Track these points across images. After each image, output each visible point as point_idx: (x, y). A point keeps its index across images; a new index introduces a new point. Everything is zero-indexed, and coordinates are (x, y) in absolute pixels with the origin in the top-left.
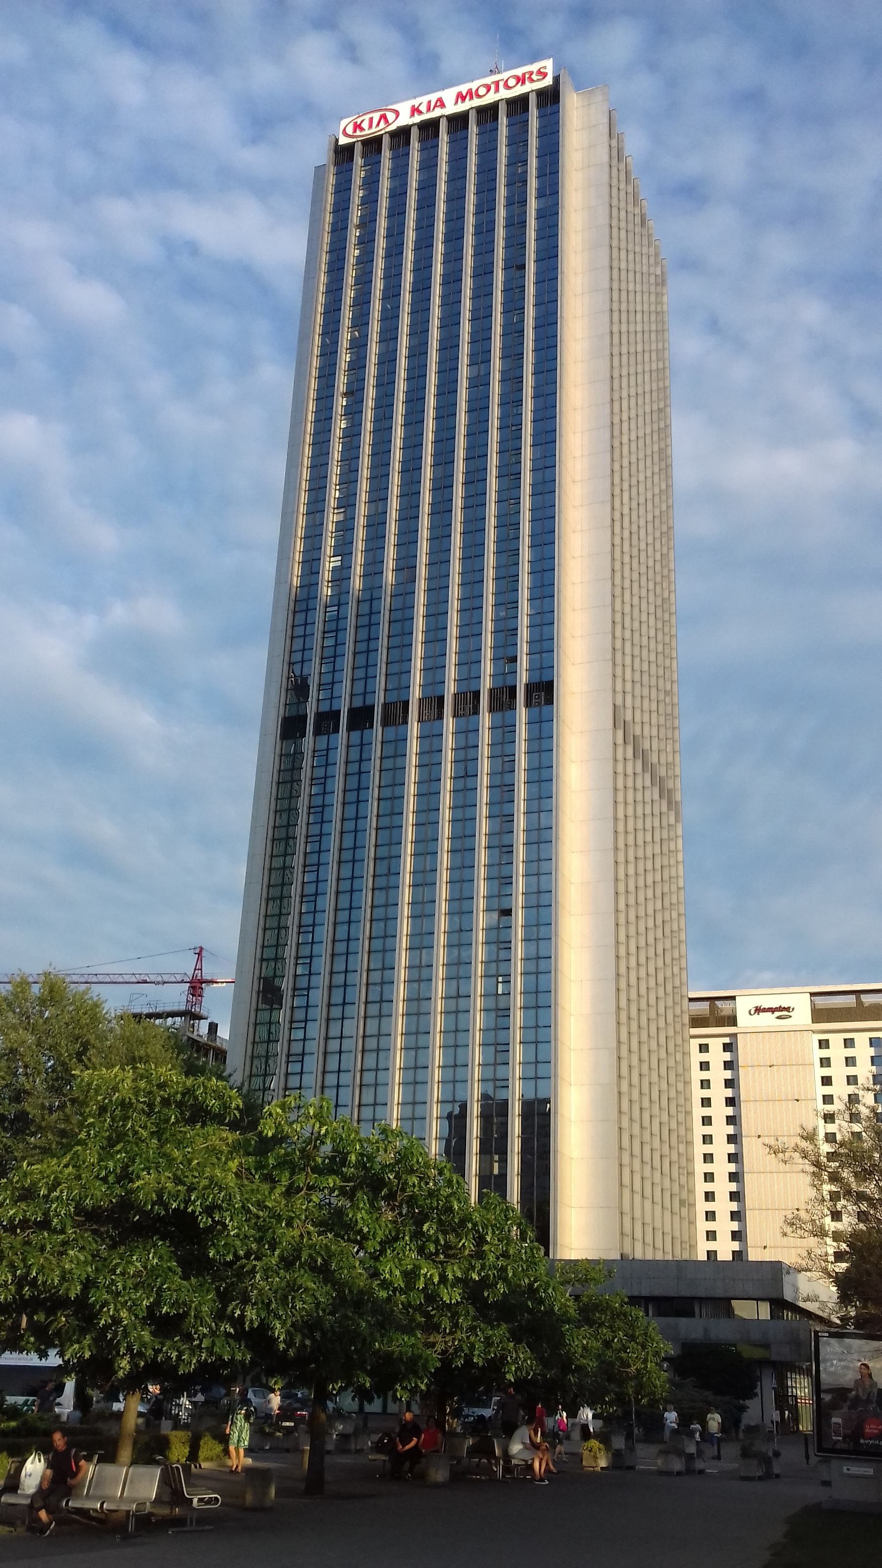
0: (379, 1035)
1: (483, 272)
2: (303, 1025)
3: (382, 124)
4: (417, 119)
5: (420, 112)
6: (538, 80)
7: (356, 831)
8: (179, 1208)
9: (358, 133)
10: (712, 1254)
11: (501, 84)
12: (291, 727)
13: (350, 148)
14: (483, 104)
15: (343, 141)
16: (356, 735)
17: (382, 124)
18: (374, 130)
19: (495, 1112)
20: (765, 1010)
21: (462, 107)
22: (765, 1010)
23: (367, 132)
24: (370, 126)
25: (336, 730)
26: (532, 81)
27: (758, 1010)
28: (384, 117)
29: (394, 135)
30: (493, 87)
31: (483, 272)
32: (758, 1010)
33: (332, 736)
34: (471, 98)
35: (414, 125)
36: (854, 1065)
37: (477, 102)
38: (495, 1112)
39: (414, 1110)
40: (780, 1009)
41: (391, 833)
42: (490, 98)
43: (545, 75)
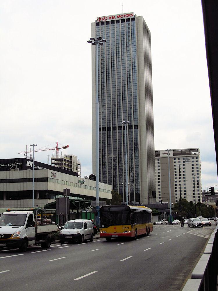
36: (185, 175)
37: (121, 19)
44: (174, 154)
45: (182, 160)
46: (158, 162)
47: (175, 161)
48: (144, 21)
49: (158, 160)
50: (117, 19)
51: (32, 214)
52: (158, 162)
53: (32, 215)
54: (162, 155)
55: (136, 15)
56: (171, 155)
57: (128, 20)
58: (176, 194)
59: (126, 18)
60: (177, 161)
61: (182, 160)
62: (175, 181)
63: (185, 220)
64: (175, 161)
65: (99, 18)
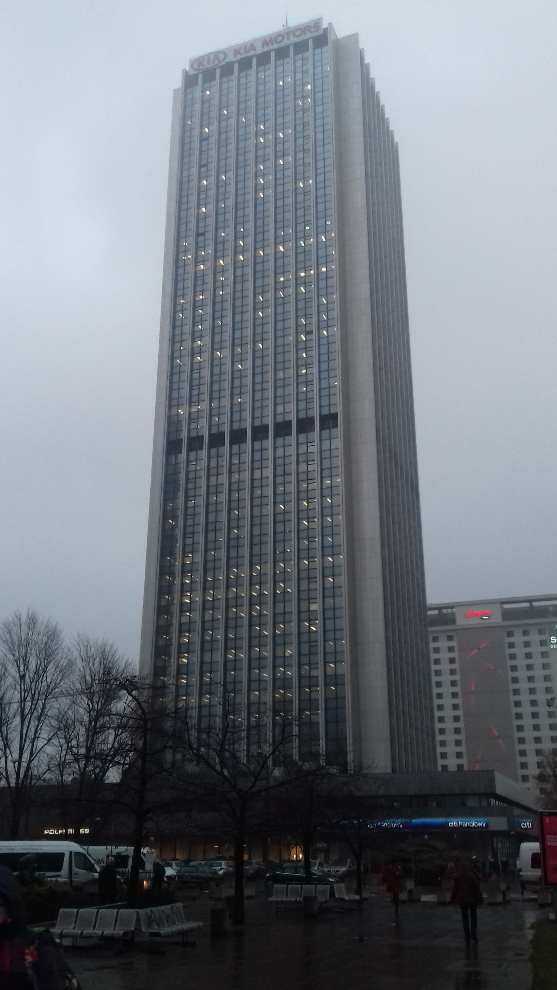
2: (198, 387)
4: (238, 58)
5: (240, 54)
6: (315, 31)
8: (50, 903)
10: (444, 767)
14: (280, 46)
18: (211, 65)
23: (207, 66)
24: (208, 64)
26: (311, 32)
29: (222, 68)
30: (286, 36)
33: (220, 449)
34: (272, 44)
35: (236, 61)
36: (550, 681)
37: (276, 46)
39: (259, 663)
41: (218, 450)
44: (506, 615)
45: (534, 637)
46: (451, 644)
47: (511, 640)
48: (365, 70)
49: (450, 638)
50: (259, 50)
51: (64, 854)
52: (451, 644)
53: (127, 857)
54: (461, 621)
55: (330, 24)
56: (497, 619)
57: (301, 47)
58: (514, 668)
59: (293, 40)
60: (518, 639)
61: (534, 637)
62: (518, 752)
63: (108, 774)
64: (511, 640)
65: (198, 62)
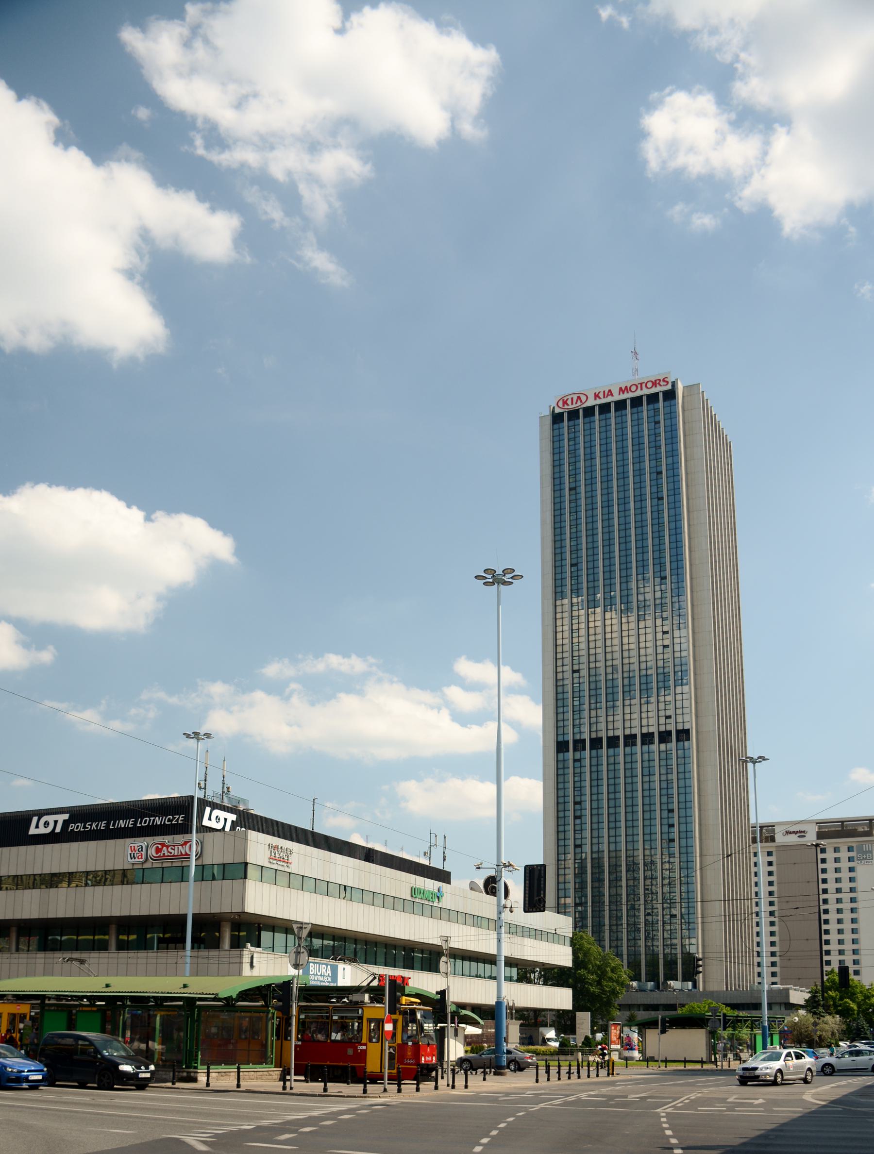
0: (651, 834)
1: (608, 543)
3: (579, 403)
4: (599, 402)
7: (564, 789)
9: (566, 407)
11: (644, 385)
12: (561, 747)
13: (592, 408)
15: (557, 410)
16: (594, 752)
17: (579, 403)
18: (574, 406)
19: (597, 864)
20: (791, 833)
21: (623, 397)
22: (791, 833)
23: (571, 407)
25: (568, 751)
27: (788, 833)
28: (579, 398)
31: (608, 543)
32: (788, 833)
38: (597, 864)
40: (801, 832)
42: (638, 393)
43: (667, 382)
